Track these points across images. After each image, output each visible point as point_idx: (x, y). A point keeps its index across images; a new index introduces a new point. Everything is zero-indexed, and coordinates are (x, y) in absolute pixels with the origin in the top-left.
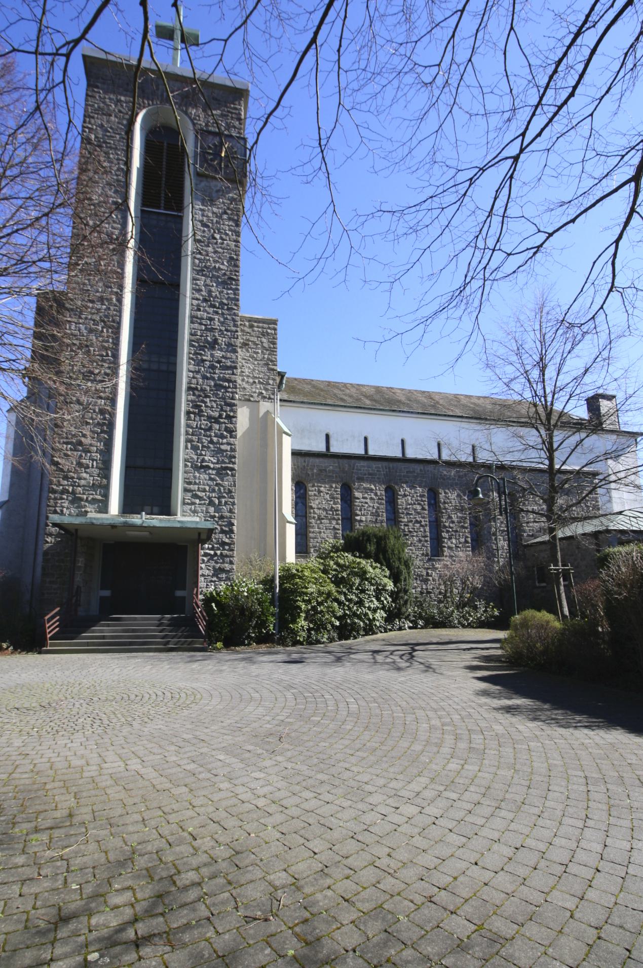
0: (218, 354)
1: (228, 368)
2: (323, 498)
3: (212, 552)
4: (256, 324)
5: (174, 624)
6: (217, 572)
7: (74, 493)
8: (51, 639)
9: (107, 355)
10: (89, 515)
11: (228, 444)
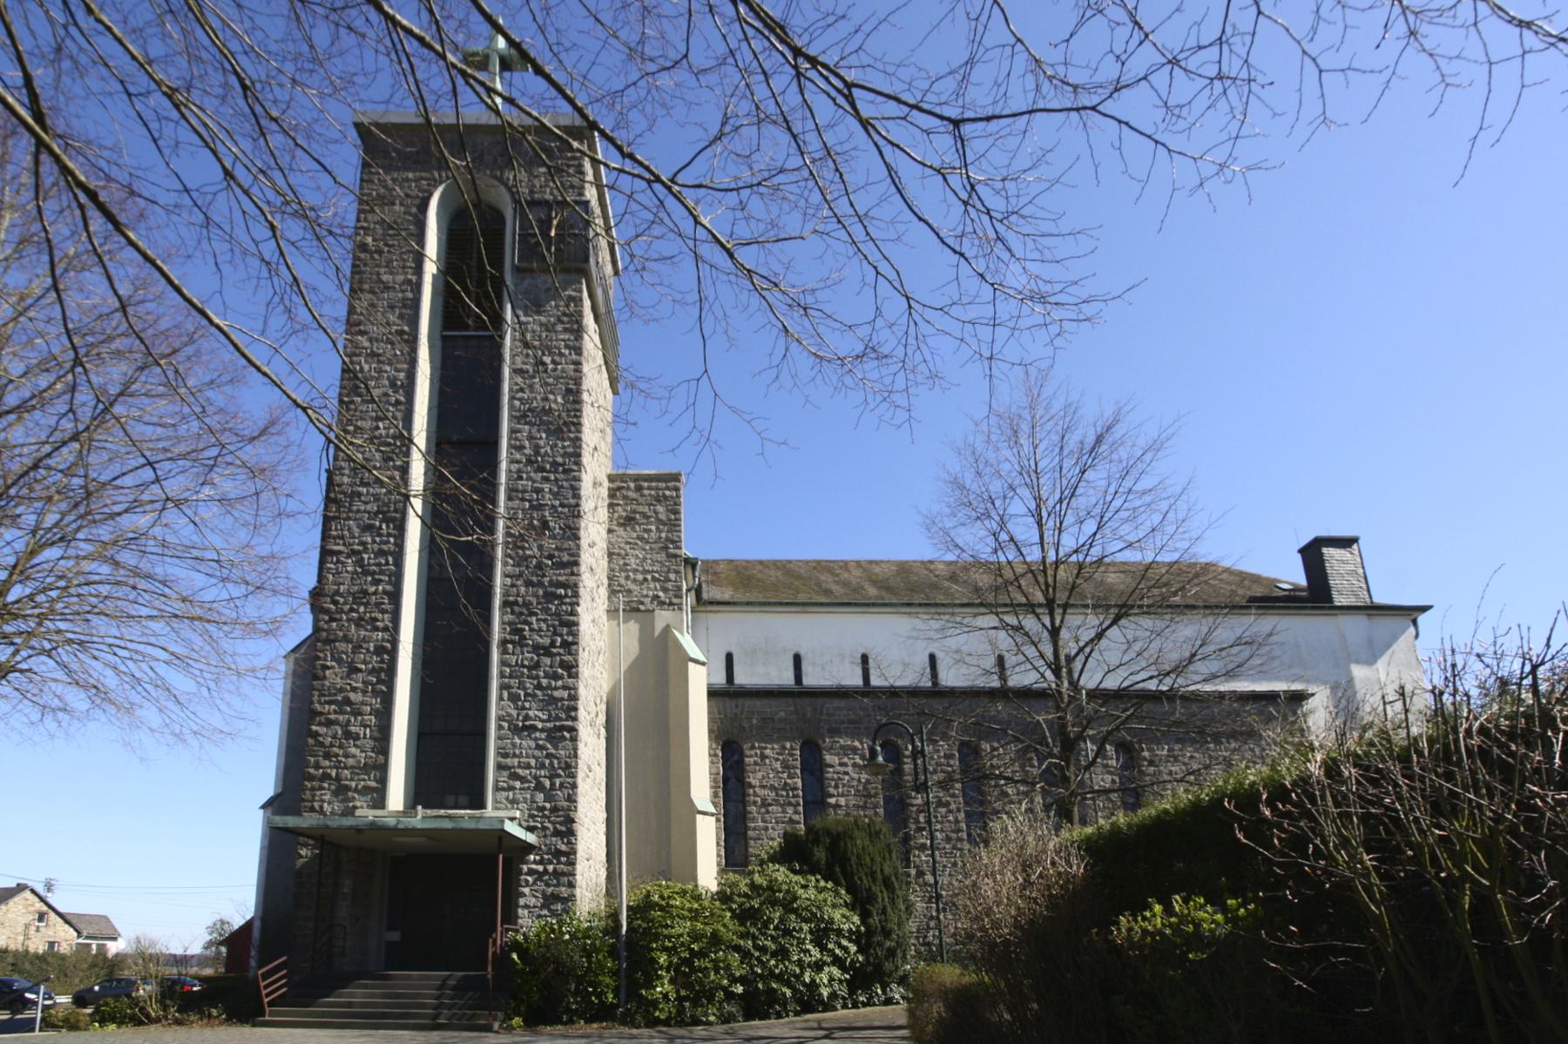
0: (550, 545)
1: (563, 565)
2: (771, 768)
3: (540, 868)
4: (646, 484)
5: (462, 987)
6: (549, 900)
7: (338, 778)
8: (271, 1004)
9: (387, 563)
10: (358, 812)
11: (565, 688)
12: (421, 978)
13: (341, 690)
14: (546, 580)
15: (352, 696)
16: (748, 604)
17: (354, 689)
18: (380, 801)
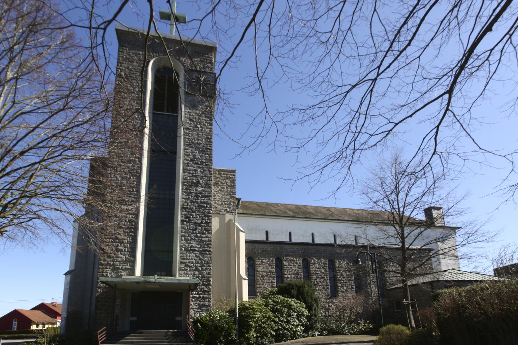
0: (200, 189)
1: (205, 196)
2: (265, 266)
3: (198, 296)
7: (114, 265)
9: (133, 191)
10: (123, 277)
11: (207, 237)
12: (156, 333)
14: (199, 201)
15: (119, 236)
16: (251, 214)
18: (132, 272)
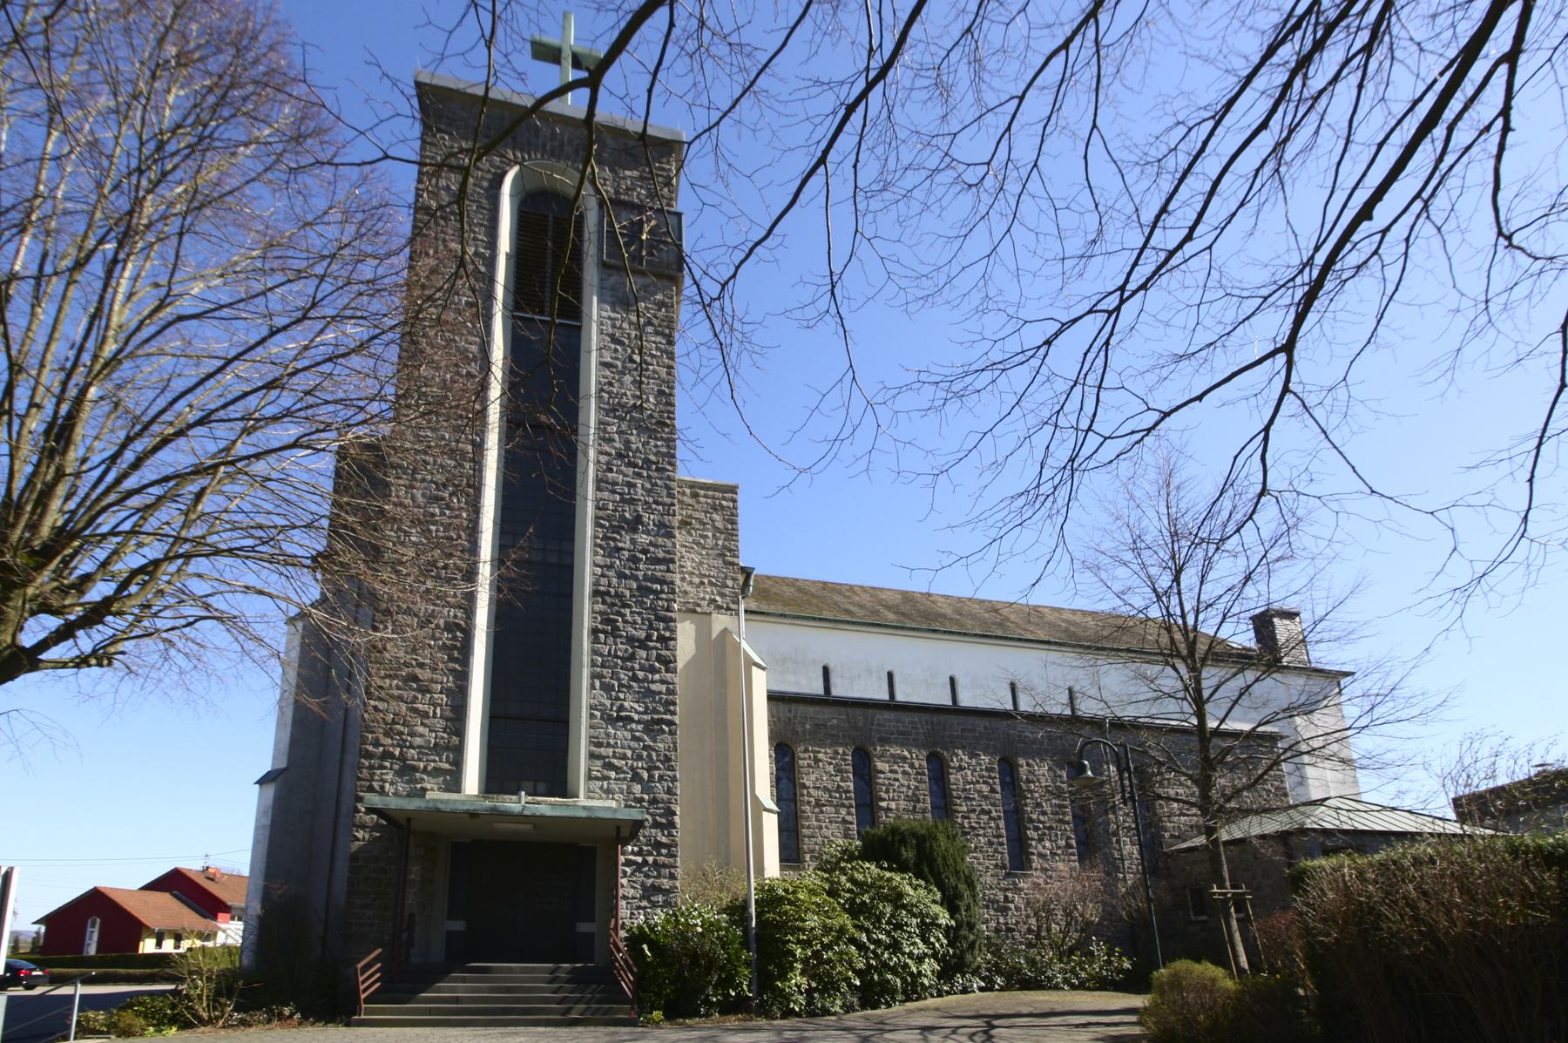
0: (643, 539)
1: (658, 561)
2: (824, 771)
3: (639, 859)
5: (578, 979)
6: (649, 892)
7: (403, 758)
8: (367, 1001)
9: (459, 537)
10: (429, 795)
11: (663, 682)
13: (406, 665)
16: (782, 615)
17: (421, 665)
18: (455, 784)
